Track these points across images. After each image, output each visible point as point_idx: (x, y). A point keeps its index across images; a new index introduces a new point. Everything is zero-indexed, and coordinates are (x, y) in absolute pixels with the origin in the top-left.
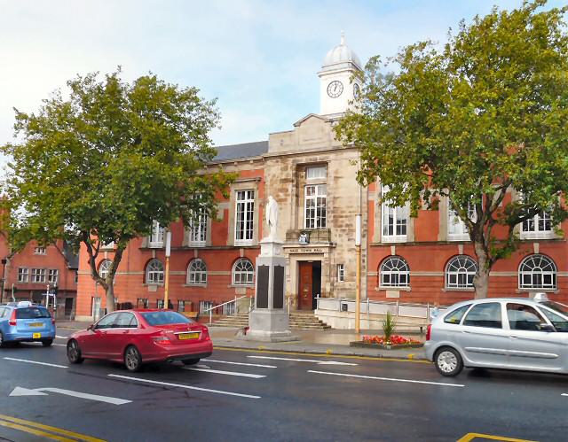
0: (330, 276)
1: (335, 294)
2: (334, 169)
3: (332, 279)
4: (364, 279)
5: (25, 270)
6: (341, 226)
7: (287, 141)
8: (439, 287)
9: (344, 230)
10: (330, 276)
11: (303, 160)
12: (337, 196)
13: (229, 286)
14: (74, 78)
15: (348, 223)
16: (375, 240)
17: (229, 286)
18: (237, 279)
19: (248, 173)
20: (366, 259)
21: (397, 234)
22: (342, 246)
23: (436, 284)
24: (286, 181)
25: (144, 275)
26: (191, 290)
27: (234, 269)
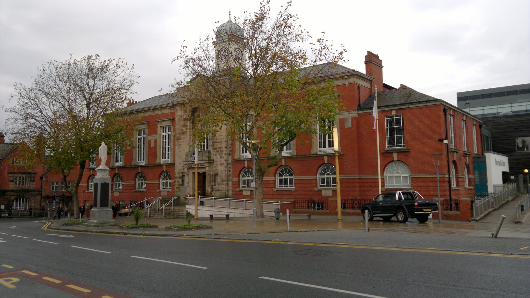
0: (210, 182)
1: (213, 194)
4: (230, 183)
5: (57, 183)
6: (216, 149)
8: (272, 187)
9: (218, 151)
10: (210, 182)
15: (219, 146)
16: (236, 157)
17: (158, 191)
18: (323, 182)
19: (167, 114)
20: (231, 170)
21: (329, 147)
22: (217, 161)
24: (185, 120)
26: (137, 194)
27: (277, 175)
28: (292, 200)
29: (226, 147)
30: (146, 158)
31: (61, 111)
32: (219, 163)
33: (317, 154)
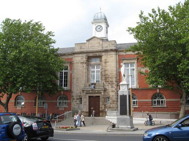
2: (105, 59)
6: (108, 82)
7: (83, 47)
9: (110, 83)
11: (91, 55)
12: (106, 69)
23: (148, 105)
29: (116, 81)
31: (167, 56)
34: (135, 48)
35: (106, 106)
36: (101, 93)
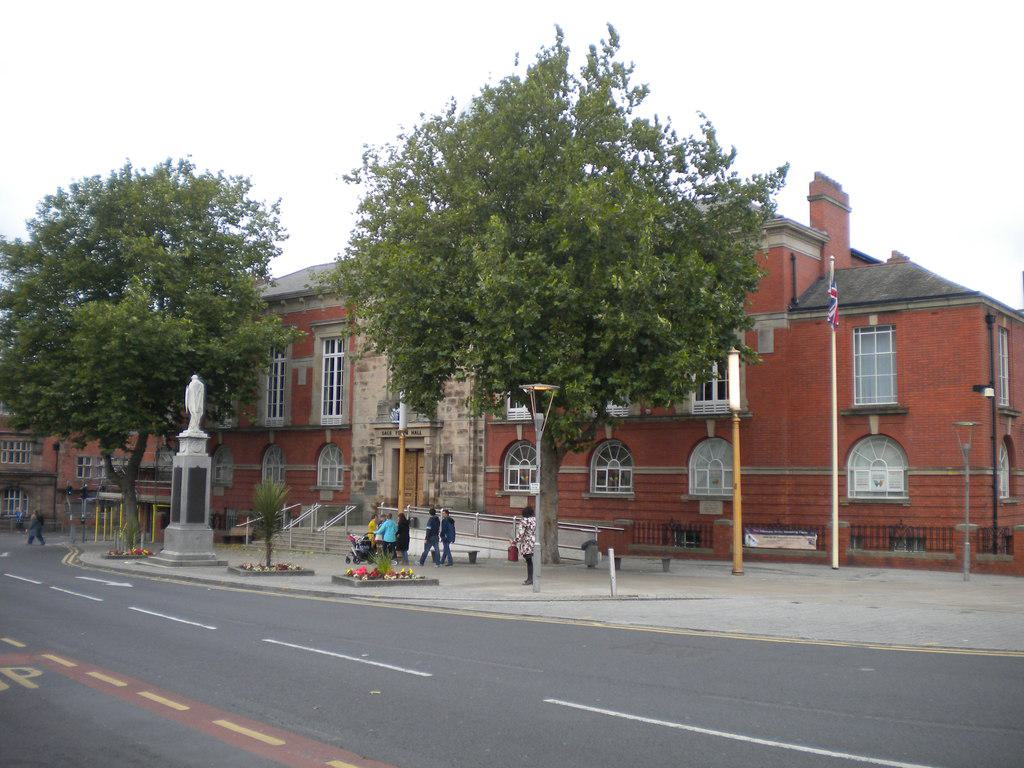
3: (437, 476)
4: (481, 477)
5: (88, 460)
9: (453, 401)
13: (312, 488)
14: (502, 79)
15: (458, 389)
17: (312, 488)
18: (513, 478)
22: (450, 425)
23: (575, 487)
25: (501, 474)
28: (628, 522)
30: (287, 410)
32: (455, 428)
33: (689, 415)
34: (194, 178)
35: (441, 487)
36: (423, 438)
